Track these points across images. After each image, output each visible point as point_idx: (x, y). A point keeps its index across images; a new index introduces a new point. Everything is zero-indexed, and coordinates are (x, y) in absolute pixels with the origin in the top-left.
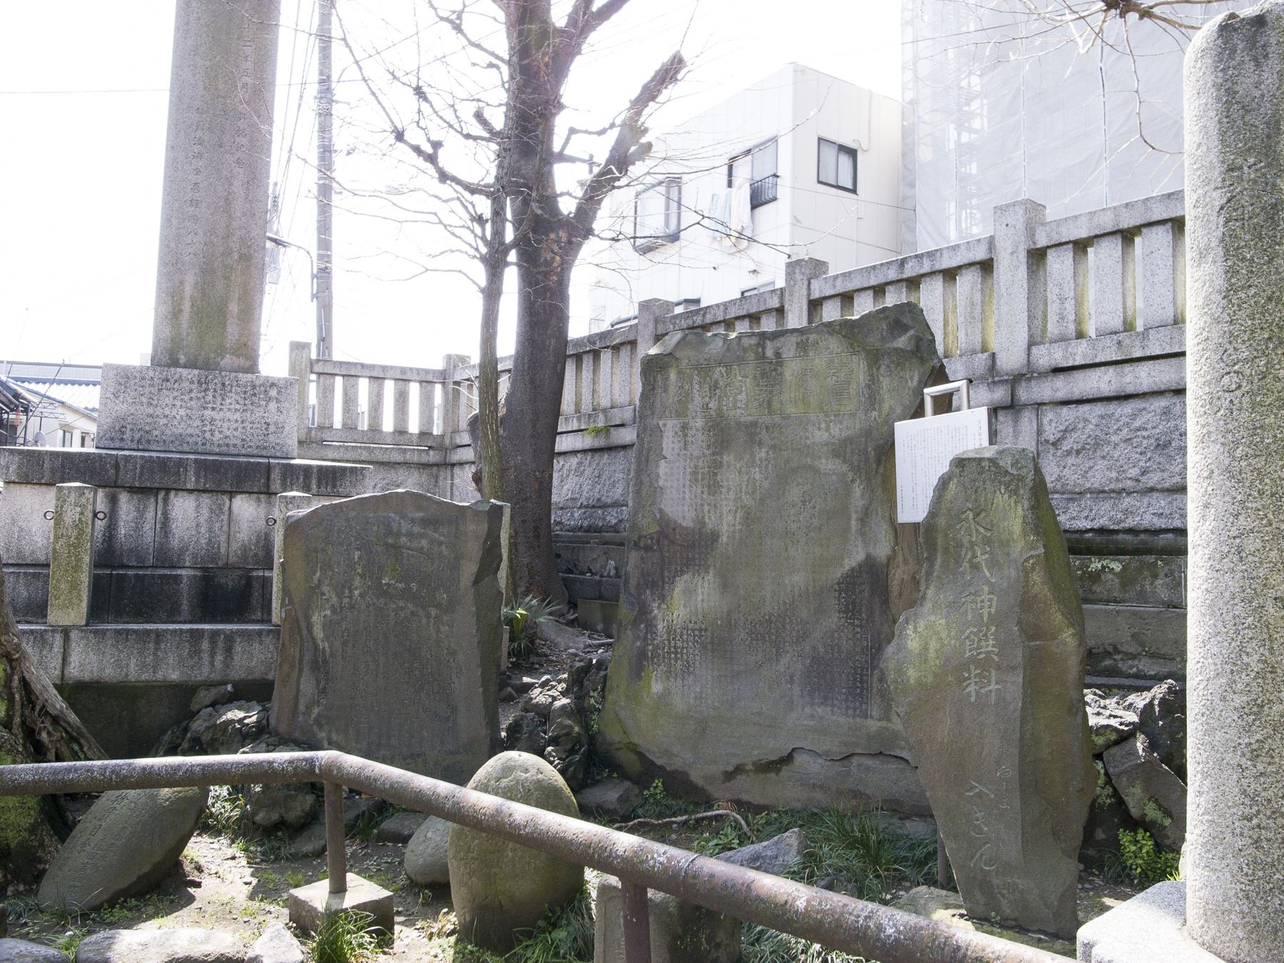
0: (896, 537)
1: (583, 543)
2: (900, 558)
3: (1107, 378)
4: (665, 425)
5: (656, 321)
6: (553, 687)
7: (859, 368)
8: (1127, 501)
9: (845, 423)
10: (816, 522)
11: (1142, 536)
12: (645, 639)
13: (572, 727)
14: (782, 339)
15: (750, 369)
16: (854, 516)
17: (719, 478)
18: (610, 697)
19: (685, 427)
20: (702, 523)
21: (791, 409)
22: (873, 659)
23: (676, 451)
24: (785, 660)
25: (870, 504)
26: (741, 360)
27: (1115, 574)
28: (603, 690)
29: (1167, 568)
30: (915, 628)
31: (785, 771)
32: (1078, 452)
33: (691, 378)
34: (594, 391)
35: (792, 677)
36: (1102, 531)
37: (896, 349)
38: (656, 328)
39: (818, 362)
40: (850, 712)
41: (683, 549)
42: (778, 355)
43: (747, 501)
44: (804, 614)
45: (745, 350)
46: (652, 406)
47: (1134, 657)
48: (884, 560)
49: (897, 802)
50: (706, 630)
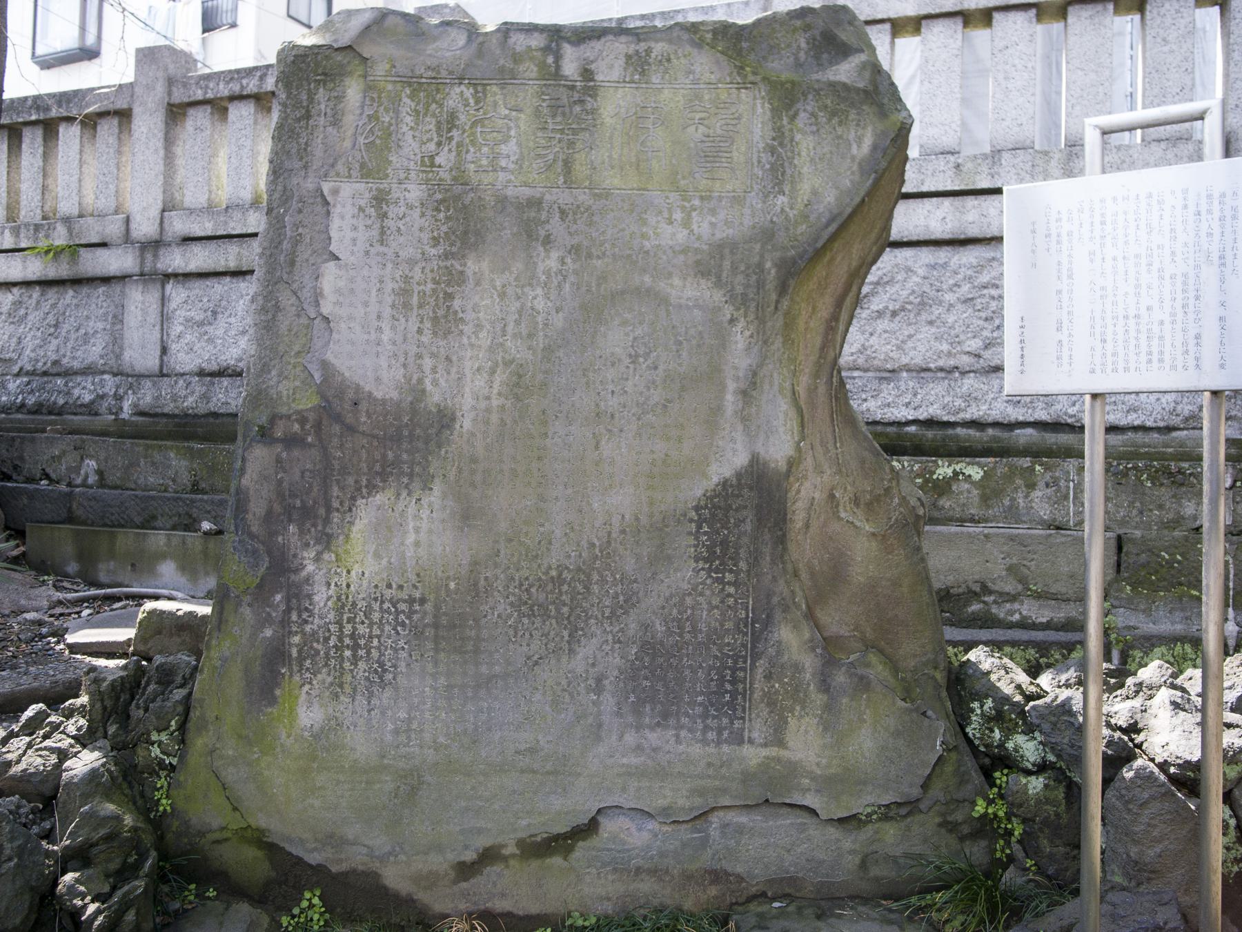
0: (802, 425)
1: (30, 431)
2: (809, 462)
3: (939, 214)
4: (335, 192)
5: (170, 82)
6: (56, 727)
7: (754, 115)
8: (969, 383)
9: (722, 215)
10: (656, 396)
11: (990, 431)
12: (285, 622)
13: (118, 819)
14: (597, 45)
15: (528, 95)
16: (731, 386)
17: (457, 304)
18: (199, 743)
19: (380, 199)
20: (419, 393)
21: (612, 180)
22: (756, 639)
23: (361, 245)
24: (587, 649)
25: (761, 365)
26: (507, 77)
27: (973, 483)
28: (182, 727)
29: (1048, 476)
31: (582, 850)
32: (894, 314)
33: (396, 100)
34: (44, 189)
35: (599, 680)
36: (930, 423)
37: (832, 85)
38: (170, 94)
39: (670, 95)
40: (711, 735)
41: (403, 442)
42: (587, 74)
43: (516, 349)
44: (630, 565)
45: (517, 58)
46: (304, 152)
47: (1013, 598)
48: (783, 466)
49: (792, 880)
50: (423, 601)
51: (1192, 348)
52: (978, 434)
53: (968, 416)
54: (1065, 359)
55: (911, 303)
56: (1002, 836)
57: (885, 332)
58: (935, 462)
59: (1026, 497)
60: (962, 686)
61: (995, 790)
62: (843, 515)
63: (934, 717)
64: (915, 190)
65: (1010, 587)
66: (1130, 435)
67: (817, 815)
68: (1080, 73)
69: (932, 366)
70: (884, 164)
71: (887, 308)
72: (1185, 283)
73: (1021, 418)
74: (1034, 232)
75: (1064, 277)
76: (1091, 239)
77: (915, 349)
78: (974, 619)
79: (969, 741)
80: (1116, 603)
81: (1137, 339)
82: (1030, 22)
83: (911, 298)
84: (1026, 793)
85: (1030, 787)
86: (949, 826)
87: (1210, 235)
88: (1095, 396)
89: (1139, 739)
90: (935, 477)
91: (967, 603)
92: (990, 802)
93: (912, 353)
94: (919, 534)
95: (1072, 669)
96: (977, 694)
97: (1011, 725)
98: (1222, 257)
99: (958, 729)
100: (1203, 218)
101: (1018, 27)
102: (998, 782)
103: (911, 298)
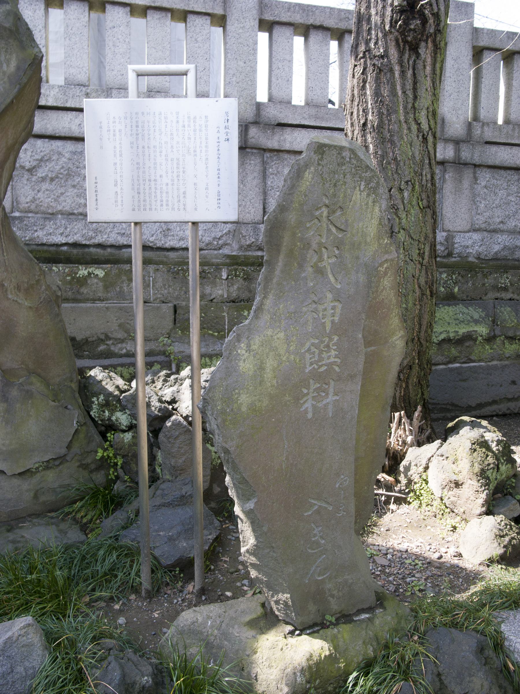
11: (109, 250)
27: (99, 279)
30: (249, 346)
32: (52, 180)
36: (75, 245)
47: (122, 341)
51: (182, 199)
52: (102, 251)
53: (96, 241)
54: (119, 202)
55: (61, 174)
56: (113, 467)
57: (47, 190)
58: (78, 267)
59: (128, 286)
60: (86, 389)
61: (108, 443)
62: (10, 296)
63: (72, 408)
64: (62, 105)
65: (120, 335)
66: (181, 252)
67: (5, 473)
68: (154, 50)
69: (76, 212)
70: (25, 80)
71: (47, 175)
72: (178, 164)
73: (125, 243)
74: (101, 127)
75: (118, 155)
76: (131, 135)
77: (65, 201)
78: (102, 354)
79: (92, 419)
80: (174, 340)
81: (155, 192)
82: (127, 14)
83: (62, 171)
84: (123, 442)
85: (125, 438)
86: (83, 466)
87: (189, 138)
88: (136, 224)
89: (176, 406)
90: (78, 276)
91: (98, 345)
92: (105, 450)
93: (64, 204)
94: (59, 307)
95: (150, 375)
96: (95, 393)
97: (113, 408)
98: (195, 151)
99: (86, 413)
100: (186, 128)
101: (120, 15)
102: (109, 438)
103: (62, 171)
